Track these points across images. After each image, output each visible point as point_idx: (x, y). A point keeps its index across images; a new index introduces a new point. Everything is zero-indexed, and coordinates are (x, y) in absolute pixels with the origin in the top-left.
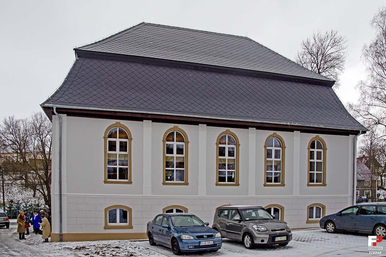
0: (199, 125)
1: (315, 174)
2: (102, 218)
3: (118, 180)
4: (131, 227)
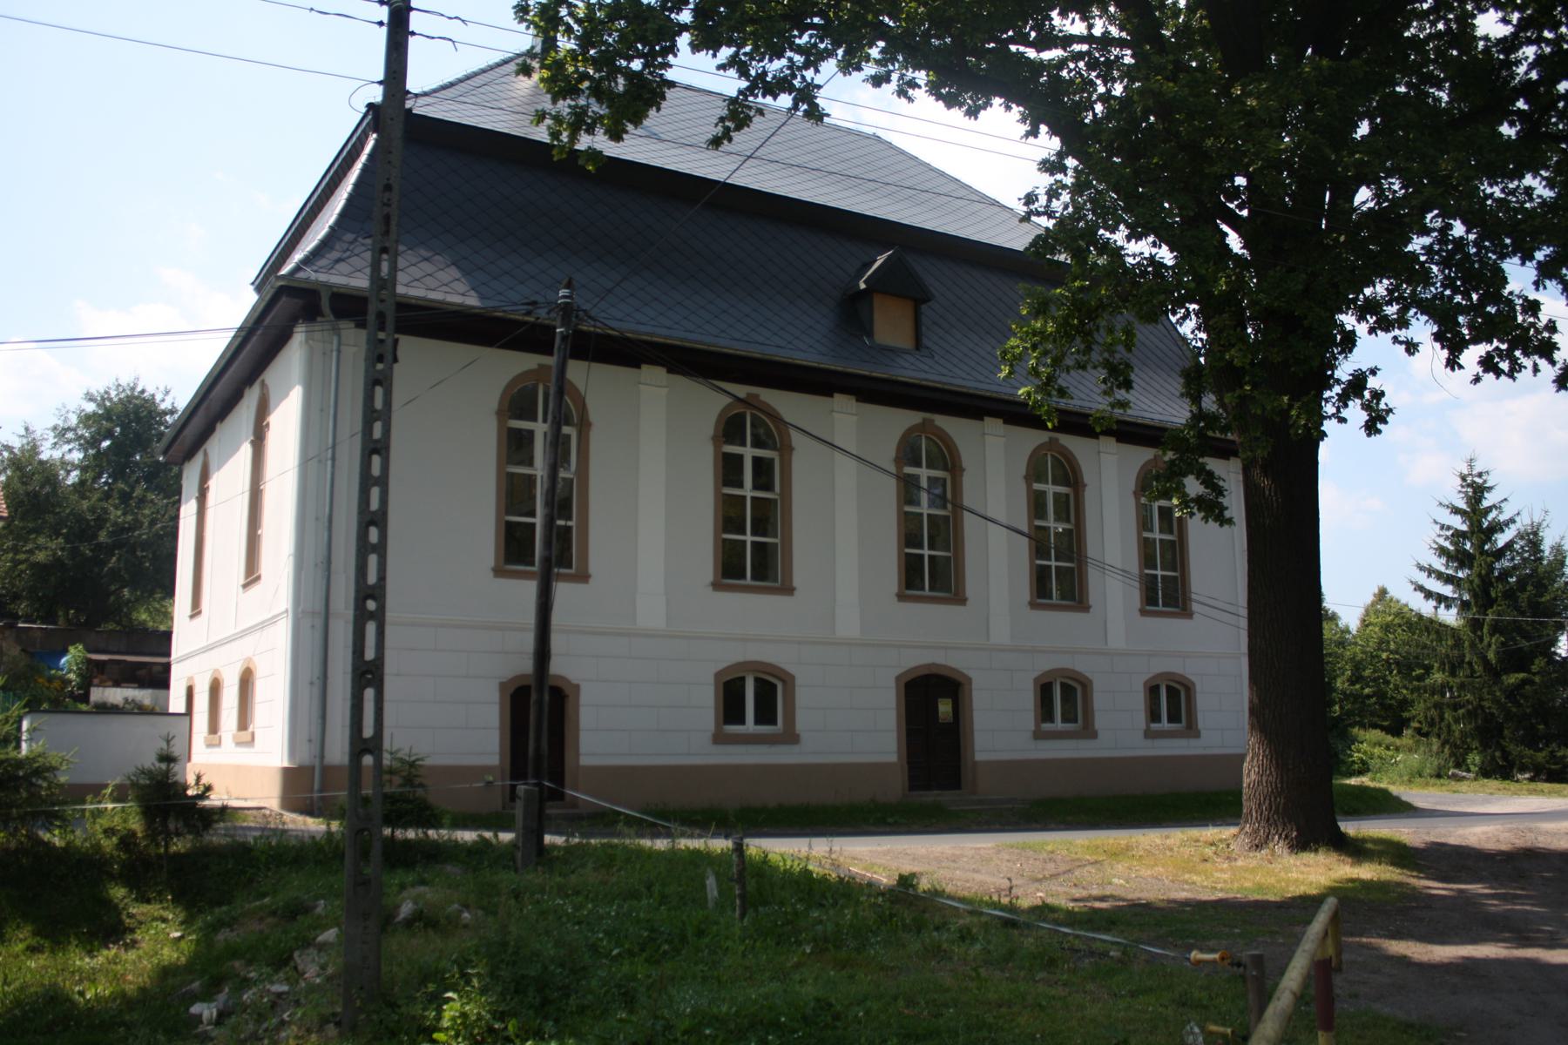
0: (982, 420)
1: (933, 553)
2: (706, 700)
3: (1161, 608)
4: (791, 737)
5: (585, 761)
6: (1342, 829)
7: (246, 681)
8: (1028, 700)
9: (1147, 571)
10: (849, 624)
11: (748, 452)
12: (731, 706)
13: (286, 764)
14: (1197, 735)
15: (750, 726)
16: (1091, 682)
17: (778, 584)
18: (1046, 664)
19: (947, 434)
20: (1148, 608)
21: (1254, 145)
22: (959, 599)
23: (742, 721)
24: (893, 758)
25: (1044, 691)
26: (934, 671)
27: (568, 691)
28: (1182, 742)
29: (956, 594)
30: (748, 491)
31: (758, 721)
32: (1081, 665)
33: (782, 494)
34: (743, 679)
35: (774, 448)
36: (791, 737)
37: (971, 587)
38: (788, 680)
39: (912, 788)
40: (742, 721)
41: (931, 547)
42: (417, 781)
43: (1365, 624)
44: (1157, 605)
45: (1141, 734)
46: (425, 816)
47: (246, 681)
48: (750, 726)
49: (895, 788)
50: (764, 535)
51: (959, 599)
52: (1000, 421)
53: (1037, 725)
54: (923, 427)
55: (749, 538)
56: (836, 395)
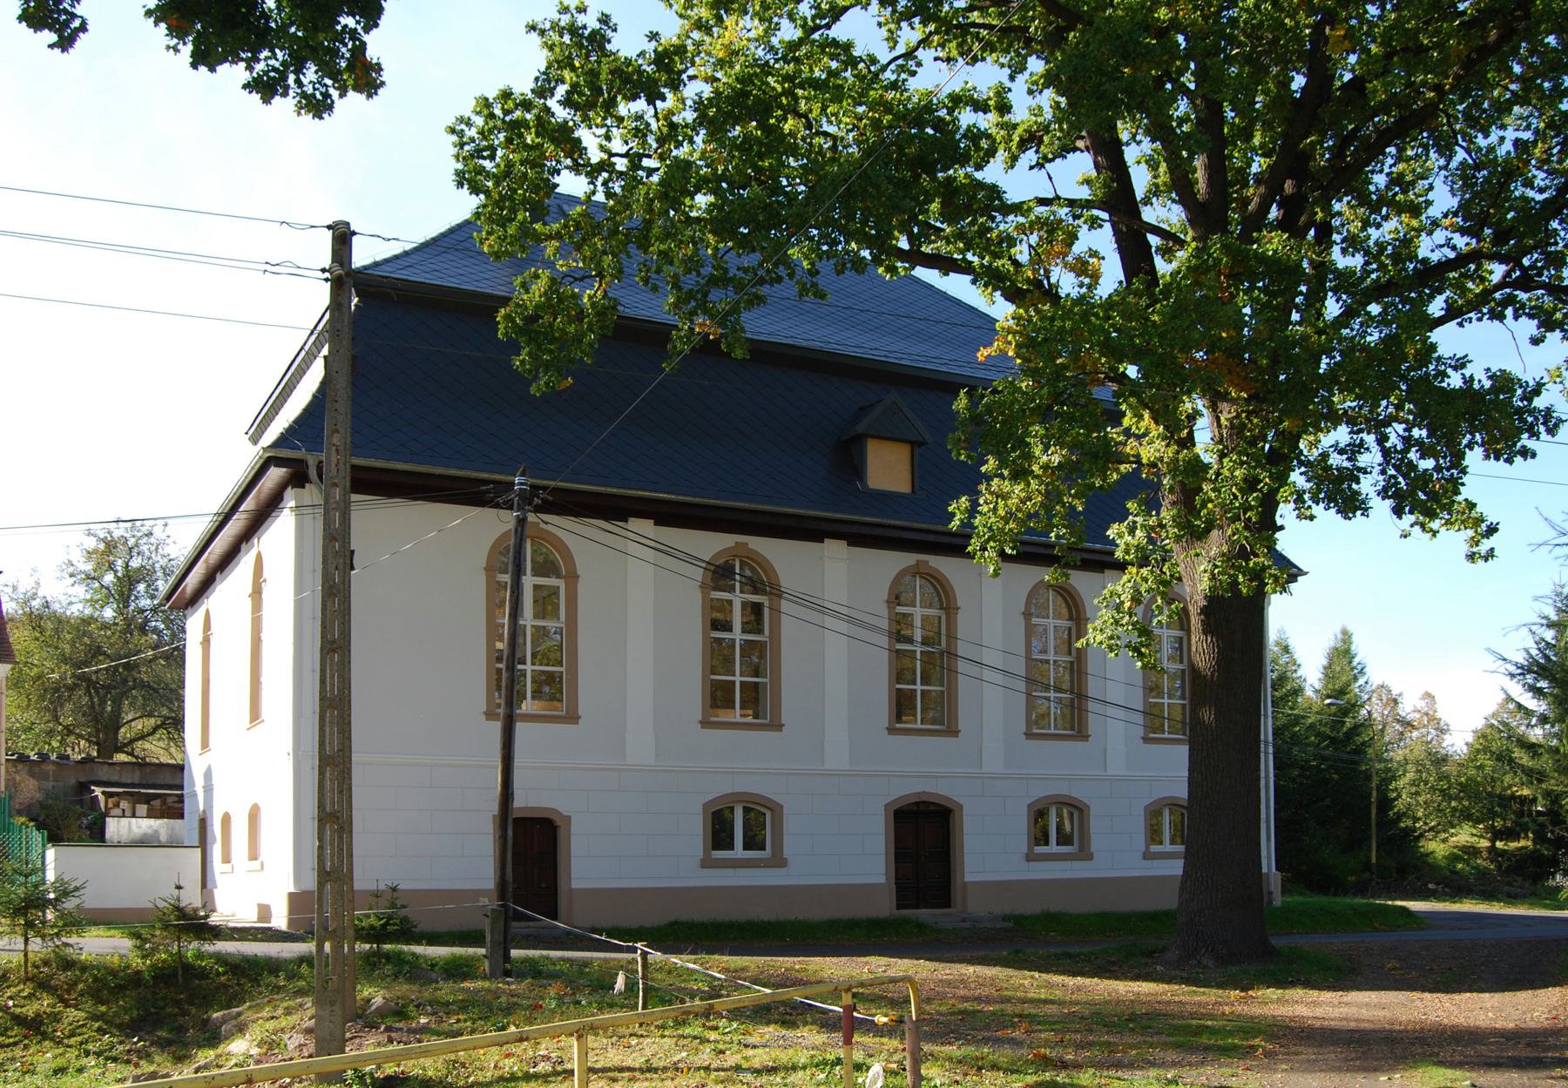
2: (696, 829)
3: (1166, 735)
4: (779, 861)
5: (575, 884)
6: (1273, 942)
7: (254, 815)
8: (1021, 825)
9: (898, 686)
10: (837, 755)
11: (738, 598)
12: (719, 831)
13: (292, 890)
14: (1090, 857)
15: (739, 851)
16: (1088, 807)
17: (767, 721)
18: (1040, 791)
19: (757, 553)
20: (1152, 735)
21: (775, 173)
22: (953, 732)
23: (731, 846)
24: (882, 879)
25: (1039, 814)
26: (925, 799)
27: (559, 823)
28: (1077, 864)
29: (1080, 731)
30: (737, 634)
31: (746, 847)
32: (1078, 792)
33: (771, 636)
34: (732, 809)
35: (559, 576)
36: (779, 861)
37: (964, 721)
38: (776, 809)
39: (899, 907)
40: (731, 846)
41: (926, 680)
42: (399, 903)
43: (1475, 752)
44: (1163, 732)
45: (1141, 854)
46: (408, 934)
47: (254, 815)
48: (739, 851)
49: (885, 906)
50: (928, 684)
51: (953, 732)
52: (843, 544)
53: (1030, 848)
54: (917, 571)
55: (919, 687)
56: (826, 540)
